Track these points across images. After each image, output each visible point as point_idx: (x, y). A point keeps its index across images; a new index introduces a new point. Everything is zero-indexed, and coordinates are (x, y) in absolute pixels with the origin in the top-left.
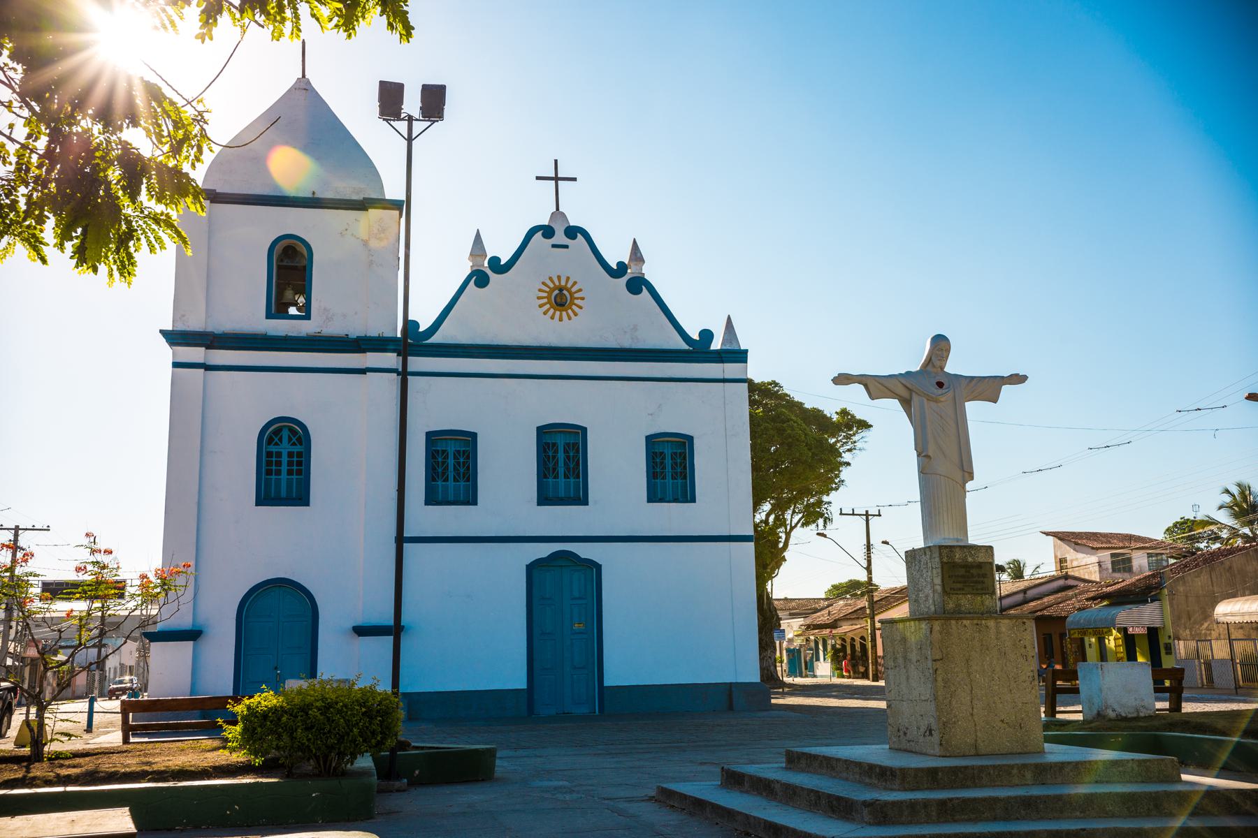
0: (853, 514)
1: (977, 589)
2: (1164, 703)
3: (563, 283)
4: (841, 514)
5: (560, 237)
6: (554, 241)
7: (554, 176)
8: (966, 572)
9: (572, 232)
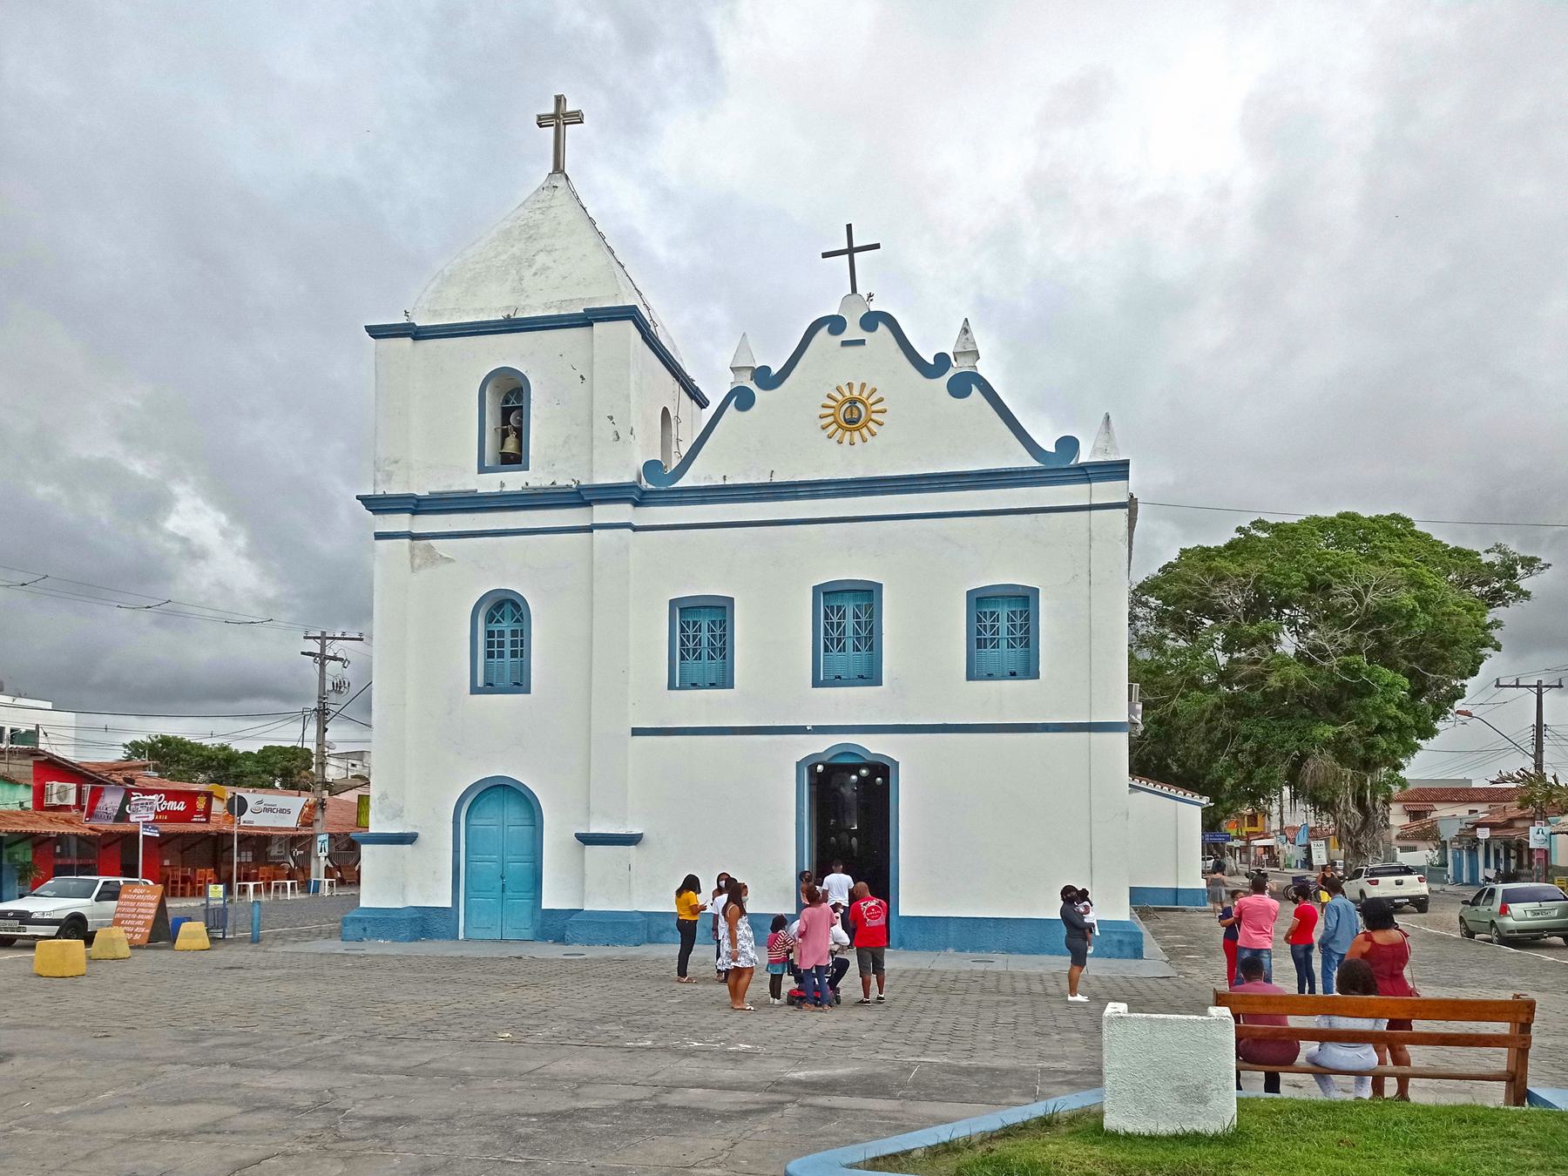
0: (1517, 686)
2: (210, 890)
3: (856, 393)
4: (1498, 686)
5: (853, 331)
6: (845, 336)
7: (855, 246)
9: (871, 321)
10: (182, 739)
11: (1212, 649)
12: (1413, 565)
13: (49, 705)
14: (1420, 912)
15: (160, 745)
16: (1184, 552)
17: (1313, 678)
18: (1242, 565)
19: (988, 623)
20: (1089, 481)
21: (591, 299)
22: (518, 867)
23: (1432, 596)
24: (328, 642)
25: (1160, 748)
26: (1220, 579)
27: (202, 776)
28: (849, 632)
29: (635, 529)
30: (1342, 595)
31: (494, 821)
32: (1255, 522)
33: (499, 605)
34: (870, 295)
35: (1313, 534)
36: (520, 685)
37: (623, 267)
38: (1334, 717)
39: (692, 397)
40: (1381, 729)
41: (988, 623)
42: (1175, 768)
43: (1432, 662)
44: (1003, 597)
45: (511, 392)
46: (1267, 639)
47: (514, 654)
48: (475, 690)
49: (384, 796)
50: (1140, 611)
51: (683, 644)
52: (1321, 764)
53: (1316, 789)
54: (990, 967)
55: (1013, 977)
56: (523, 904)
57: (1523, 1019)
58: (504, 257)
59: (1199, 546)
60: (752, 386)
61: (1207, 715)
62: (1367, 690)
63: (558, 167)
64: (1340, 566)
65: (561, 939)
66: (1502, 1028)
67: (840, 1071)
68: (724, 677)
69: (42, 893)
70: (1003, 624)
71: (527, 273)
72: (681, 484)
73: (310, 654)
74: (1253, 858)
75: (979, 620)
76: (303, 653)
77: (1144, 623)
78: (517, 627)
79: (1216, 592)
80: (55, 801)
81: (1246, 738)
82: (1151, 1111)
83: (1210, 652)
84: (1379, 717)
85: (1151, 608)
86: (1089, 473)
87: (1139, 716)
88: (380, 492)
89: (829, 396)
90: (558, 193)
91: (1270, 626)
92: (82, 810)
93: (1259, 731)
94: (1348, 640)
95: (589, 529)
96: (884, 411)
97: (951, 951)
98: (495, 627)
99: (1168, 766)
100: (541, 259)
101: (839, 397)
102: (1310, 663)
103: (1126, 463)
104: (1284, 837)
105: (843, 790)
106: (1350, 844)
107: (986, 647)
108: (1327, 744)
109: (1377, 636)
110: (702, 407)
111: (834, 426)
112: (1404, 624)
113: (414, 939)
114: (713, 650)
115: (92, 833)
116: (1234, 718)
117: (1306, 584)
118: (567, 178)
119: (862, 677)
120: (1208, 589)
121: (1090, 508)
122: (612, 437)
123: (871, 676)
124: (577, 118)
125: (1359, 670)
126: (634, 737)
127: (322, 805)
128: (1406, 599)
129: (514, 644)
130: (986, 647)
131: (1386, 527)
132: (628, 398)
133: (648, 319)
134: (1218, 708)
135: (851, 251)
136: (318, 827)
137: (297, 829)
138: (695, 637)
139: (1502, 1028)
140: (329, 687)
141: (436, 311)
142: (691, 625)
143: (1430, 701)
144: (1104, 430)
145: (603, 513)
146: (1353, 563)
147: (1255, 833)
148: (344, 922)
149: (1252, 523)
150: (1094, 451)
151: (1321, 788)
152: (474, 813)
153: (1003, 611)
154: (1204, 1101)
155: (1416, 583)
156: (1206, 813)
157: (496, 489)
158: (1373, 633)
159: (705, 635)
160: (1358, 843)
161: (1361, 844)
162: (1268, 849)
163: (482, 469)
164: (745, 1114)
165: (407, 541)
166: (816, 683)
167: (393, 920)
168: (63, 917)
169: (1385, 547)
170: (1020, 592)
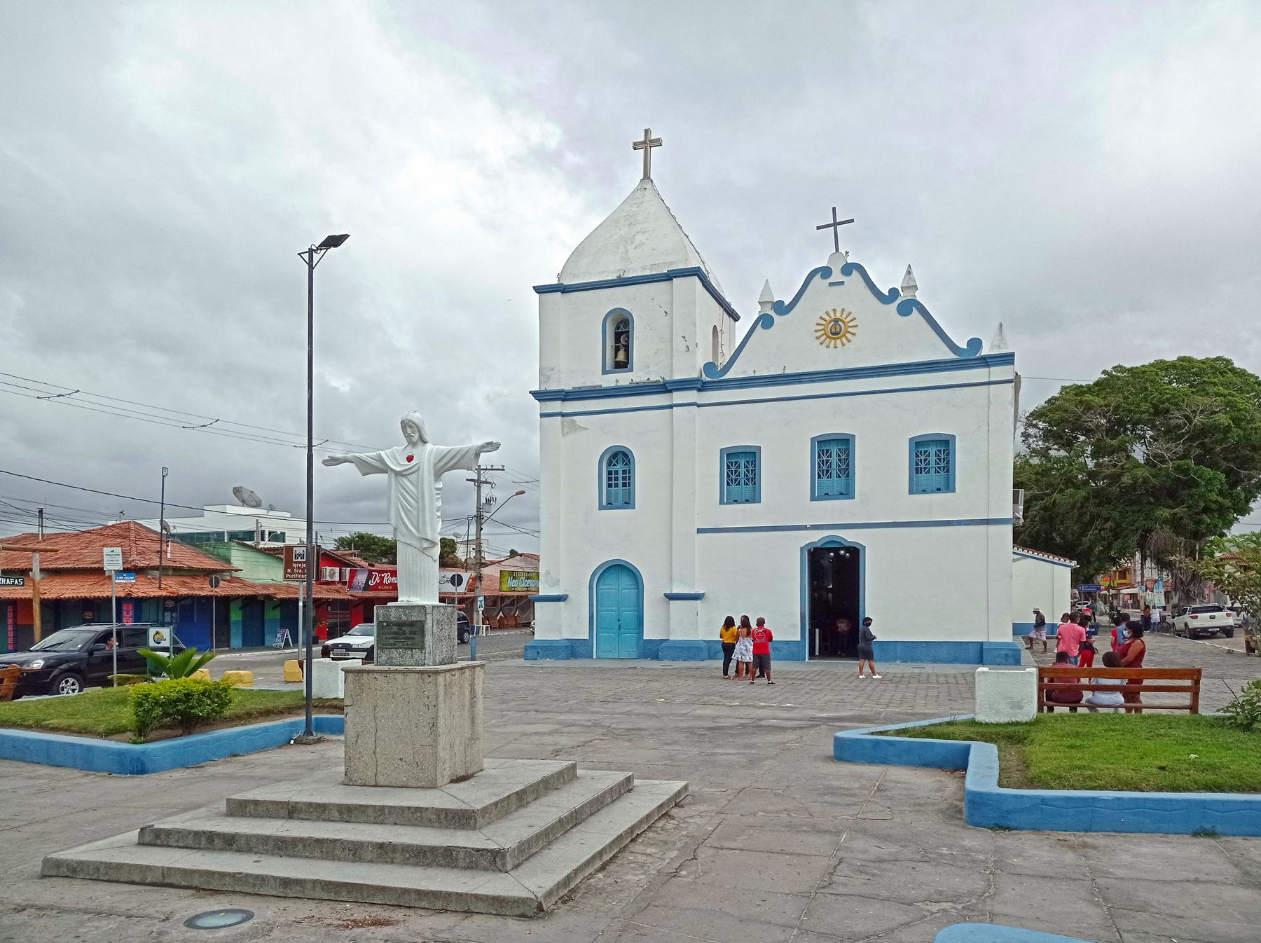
1: (407, 645)
3: (838, 315)
6: (832, 279)
8: (398, 629)
9: (848, 269)
10: (371, 535)
11: (1082, 457)
12: (1230, 394)
13: (288, 515)
14: (1228, 637)
15: (357, 539)
16: (1064, 388)
17: (1154, 477)
18: (1104, 398)
19: (923, 458)
20: (988, 366)
21: (671, 263)
22: (628, 614)
23: (1243, 416)
24: (482, 472)
25: (1045, 527)
26: (1089, 408)
27: (384, 560)
28: (834, 466)
29: (699, 406)
30: (1176, 418)
31: (613, 587)
32: (1116, 367)
33: (615, 455)
34: (847, 253)
35: (1157, 375)
36: (628, 503)
37: (687, 237)
38: (1170, 502)
39: (730, 315)
40: (1207, 510)
41: (923, 458)
42: (1058, 540)
43: (1245, 463)
44: (932, 441)
45: (621, 322)
46: (1122, 449)
47: (624, 485)
48: (601, 507)
49: (548, 573)
50: (1032, 431)
51: (728, 476)
52: (1162, 535)
53: (1159, 553)
54: (923, 671)
55: (937, 675)
56: (630, 636)
57: (1195, 678)
58: (615, 237)
59: (1074, 384)
60: (772, 313)
61: (1079, 504)
62: (1193, 483)
63: (647, 176)
64: (1176, 398)
65: (656, 657)
66: (1188, 683)
67: (843, 714)
68: (754, 495)
69: (354, 633)
70: (933, 458)
71: (630, 248)
72: (727, 376)
73: (471, 480)
74: (1121, 603)
75: (917, 456)
76: (467, 480)
77: (1034, 439)
78: (626, 468)
79: (1085, 418)
80: (328, 579)
81: (1107, 520)
82: (998, 713)
83: (1081, 459)
84: (1205, 502)
85: (1039, 429)
86: (987, 362)
87: (1021, 513)
88: (543, 389)
89: (821, 318)
90: (647, 192)
91: (1126, 438)
92: (345, 583)
93: (1116, 514)
94: (1180, 449)
95: (671, 407)
96: (856, 326)
97: (898, 662)
98: (612, 469)
99: (1053, 538)
100: (639, 238)
101: (828, 318)
102: (1154, 466)
103: (1012, 355)
104: (1144, 587)
105: (822, 562)
106: (1183, 591)
107: (921, 473)
108: (1166, 521)
109: (1203, 445)
110: (736, 320)
111: (824, 337)
112: (1222, 436)
113: (568, 658)
114: (748, 479)
115: (352, 598)
116: (1098, 505)
117: (1152, 410)
118: (652, 181)
119: (842, 494)
120: (1081, 416)
121: (989, 383)
122: (685, 349)
123: (847, 493)
124: (658, 143)
125: (1188, 469)
126: (699, 534)
127: (480, 578)
128: (1223, 419)
129: (624, 478)
130: (921, 473)
131: (1212, 367)
132: (695, 324)
133: (704, 270)
134: (1087, 499)
135: (835, 224)
136: (477, 592)
137: (465, 594)
138: (736, 472)
139: (1188, 683)
140: (483, 501)
141: (575, 274)
142: (734, 464)
143: (1244, 489)
144: (998, 332)
145: (678, 397)
146: (1186, 395)
147: (1125, 584)
148: (526, 648)
149: (1114, 368)
150: (992, 348)
151: (1162, 552)
152: (602, 580)
153: (933, 450)
154: (1021, 708)
155: (1231, 405)
156: (1075, 573)
157: (613, 385)
158: (1200, 444)
159: (742, 470)
160: (1189, 591)
161: (1191, 591)
162: (1133, 596)
163: (604, 372)
164: (802, 728)
165: (560, 418)
166: (813, 498)
167: (555, 647)
168: (369, 647)
169: (1212, 383)
170: (943, 438)
